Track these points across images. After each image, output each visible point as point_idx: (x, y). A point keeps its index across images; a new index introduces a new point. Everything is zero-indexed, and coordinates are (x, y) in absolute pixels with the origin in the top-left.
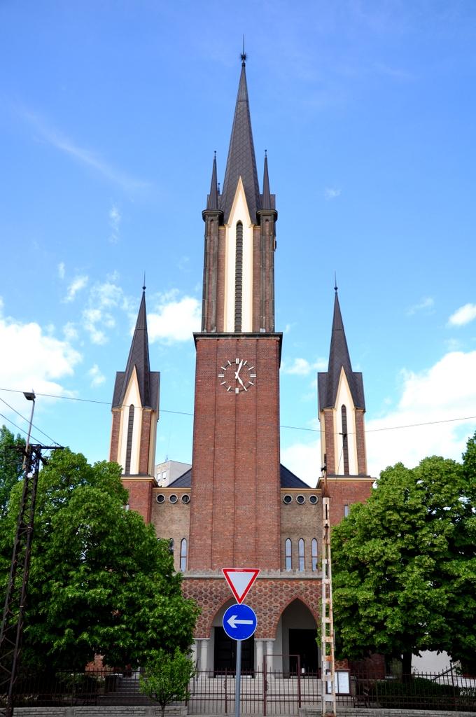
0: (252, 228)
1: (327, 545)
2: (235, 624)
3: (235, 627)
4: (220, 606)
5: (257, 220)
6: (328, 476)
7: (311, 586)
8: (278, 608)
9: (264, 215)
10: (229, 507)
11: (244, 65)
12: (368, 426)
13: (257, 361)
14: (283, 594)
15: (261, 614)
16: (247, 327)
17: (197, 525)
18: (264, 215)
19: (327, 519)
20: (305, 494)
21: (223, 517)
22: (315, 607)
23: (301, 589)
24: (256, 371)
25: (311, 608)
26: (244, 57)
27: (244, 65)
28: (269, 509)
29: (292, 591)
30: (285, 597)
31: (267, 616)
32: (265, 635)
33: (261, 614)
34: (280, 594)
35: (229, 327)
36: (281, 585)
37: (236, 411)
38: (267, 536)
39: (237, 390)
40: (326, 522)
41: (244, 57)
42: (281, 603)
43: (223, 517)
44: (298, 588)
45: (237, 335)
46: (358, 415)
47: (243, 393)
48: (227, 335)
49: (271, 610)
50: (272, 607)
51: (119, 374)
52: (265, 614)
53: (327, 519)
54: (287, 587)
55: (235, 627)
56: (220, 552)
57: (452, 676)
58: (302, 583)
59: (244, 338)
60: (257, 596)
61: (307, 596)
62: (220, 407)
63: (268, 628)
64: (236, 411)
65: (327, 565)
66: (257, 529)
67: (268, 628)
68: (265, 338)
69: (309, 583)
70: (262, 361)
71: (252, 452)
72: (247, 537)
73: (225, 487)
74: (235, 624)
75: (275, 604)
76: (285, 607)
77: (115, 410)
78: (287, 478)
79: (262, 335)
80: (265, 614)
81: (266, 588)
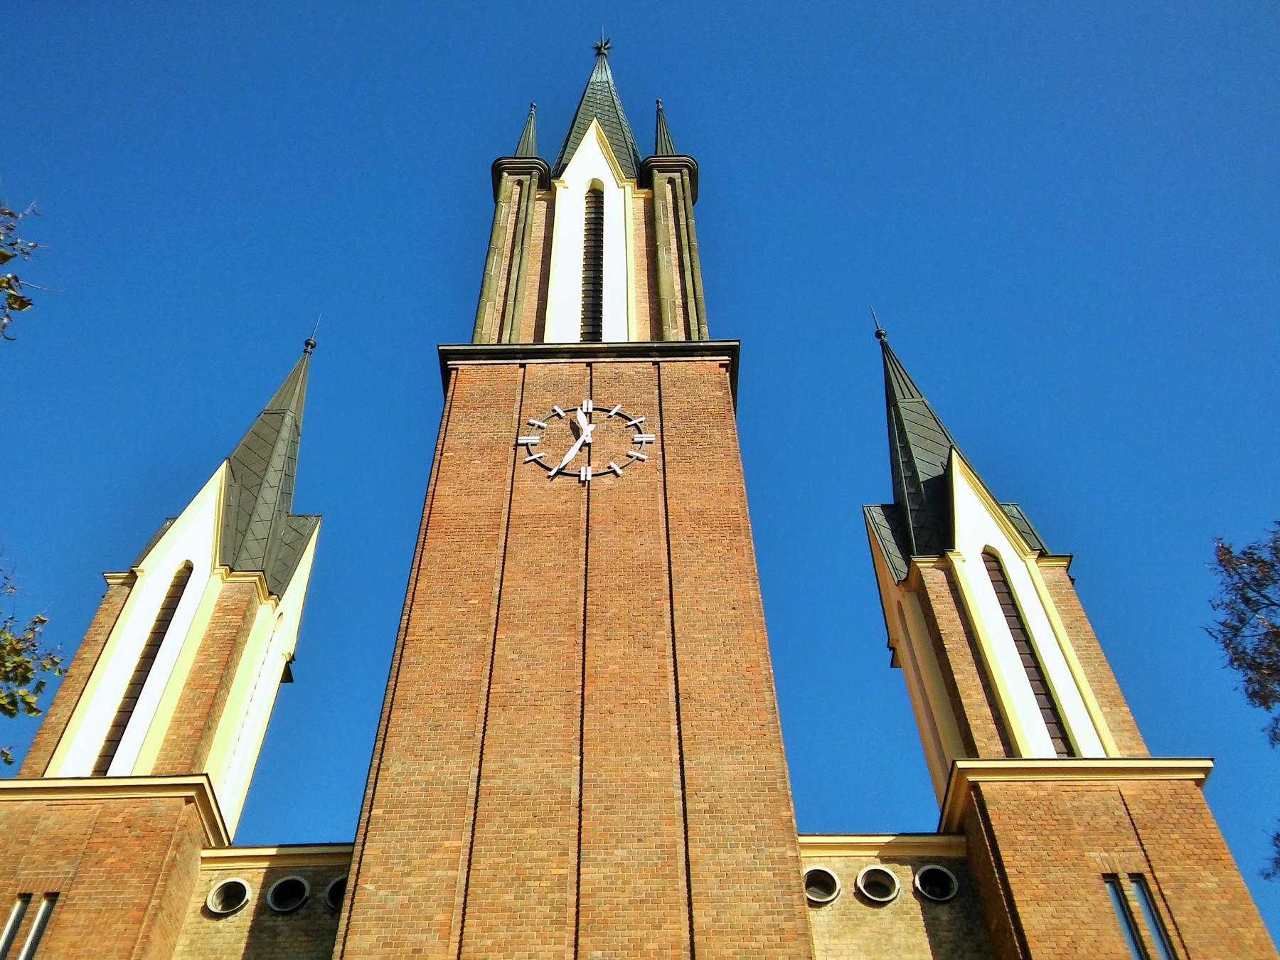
10: (543, 854)
12: (1084, 757)
21: (508, 897)
28: (743, 855)
43: (508, 897)
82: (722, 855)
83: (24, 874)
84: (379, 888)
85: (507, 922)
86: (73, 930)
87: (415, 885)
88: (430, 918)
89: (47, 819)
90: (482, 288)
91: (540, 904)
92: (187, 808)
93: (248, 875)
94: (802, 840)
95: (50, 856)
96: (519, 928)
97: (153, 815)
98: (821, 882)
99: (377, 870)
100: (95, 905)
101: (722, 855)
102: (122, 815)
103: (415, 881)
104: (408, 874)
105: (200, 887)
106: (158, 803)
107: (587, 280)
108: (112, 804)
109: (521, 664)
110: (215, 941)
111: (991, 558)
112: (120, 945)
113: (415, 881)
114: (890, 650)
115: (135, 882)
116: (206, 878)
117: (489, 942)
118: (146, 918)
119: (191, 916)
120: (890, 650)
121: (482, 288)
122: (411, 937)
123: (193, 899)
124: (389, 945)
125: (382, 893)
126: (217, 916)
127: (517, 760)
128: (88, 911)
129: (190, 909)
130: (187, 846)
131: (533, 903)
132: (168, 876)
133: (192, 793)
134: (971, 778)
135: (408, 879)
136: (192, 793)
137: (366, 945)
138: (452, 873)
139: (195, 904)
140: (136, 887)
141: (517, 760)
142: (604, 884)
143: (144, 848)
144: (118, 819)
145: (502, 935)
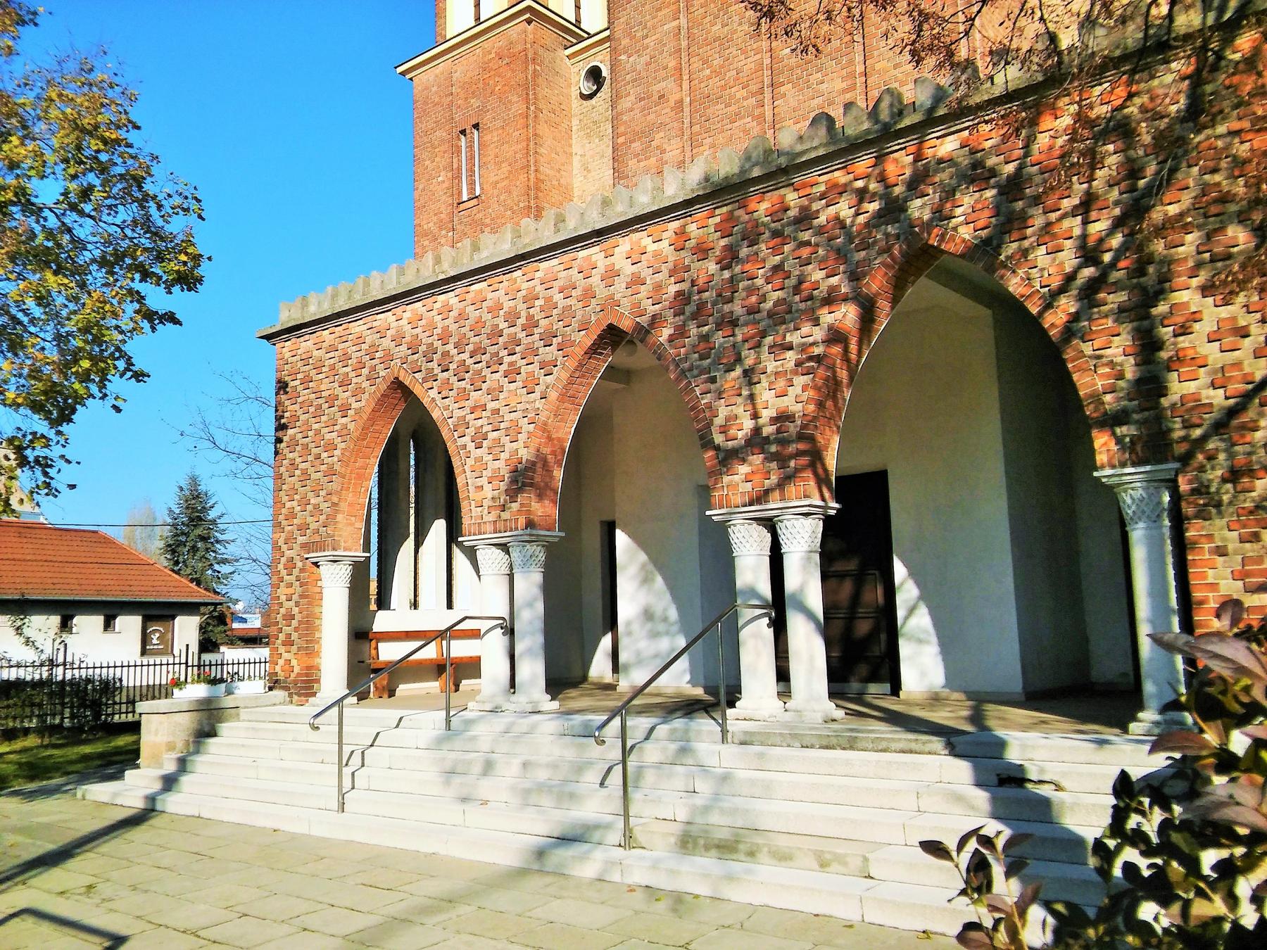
83: (457, 117)
85: (718, 50)
86: (492, 146)
87: (652, 44)
88: (665, 68)
89: (456, 72)
91: (740, 24)
92: (530, 28)
93: (600, 57)
95: (466, 99)
96: (727, 51)
97: (511, 43)
100: (499, 123)
102: (494, 51)
104: (647, 36)
105: (574, 80)
106: (511, 32)
108: (485, 45)
110: (593, 115)
112: (520, 146)
114: (62, 194)
115: (515, 99)
116: (576, 70)
117: (708, 72)
119: (576, 103)
120: (62, 194)
122: (656, 88)
123: (573, 89)
124: (643, 99)
125: (631, 59)
126: (591, 96)
128: (497, 129)
129: (574, 97)
130: (548, 56)
131: (735, 25)
132: (535, 85)
133: (528, 16)
135: (646, 41)
136: (528, 16)
137: (629, 105)
138: (675, 23)
139: (575, 93)
140: (517, 102)
143: (513, 71)
144: (493, 55)
145: (715, 62)
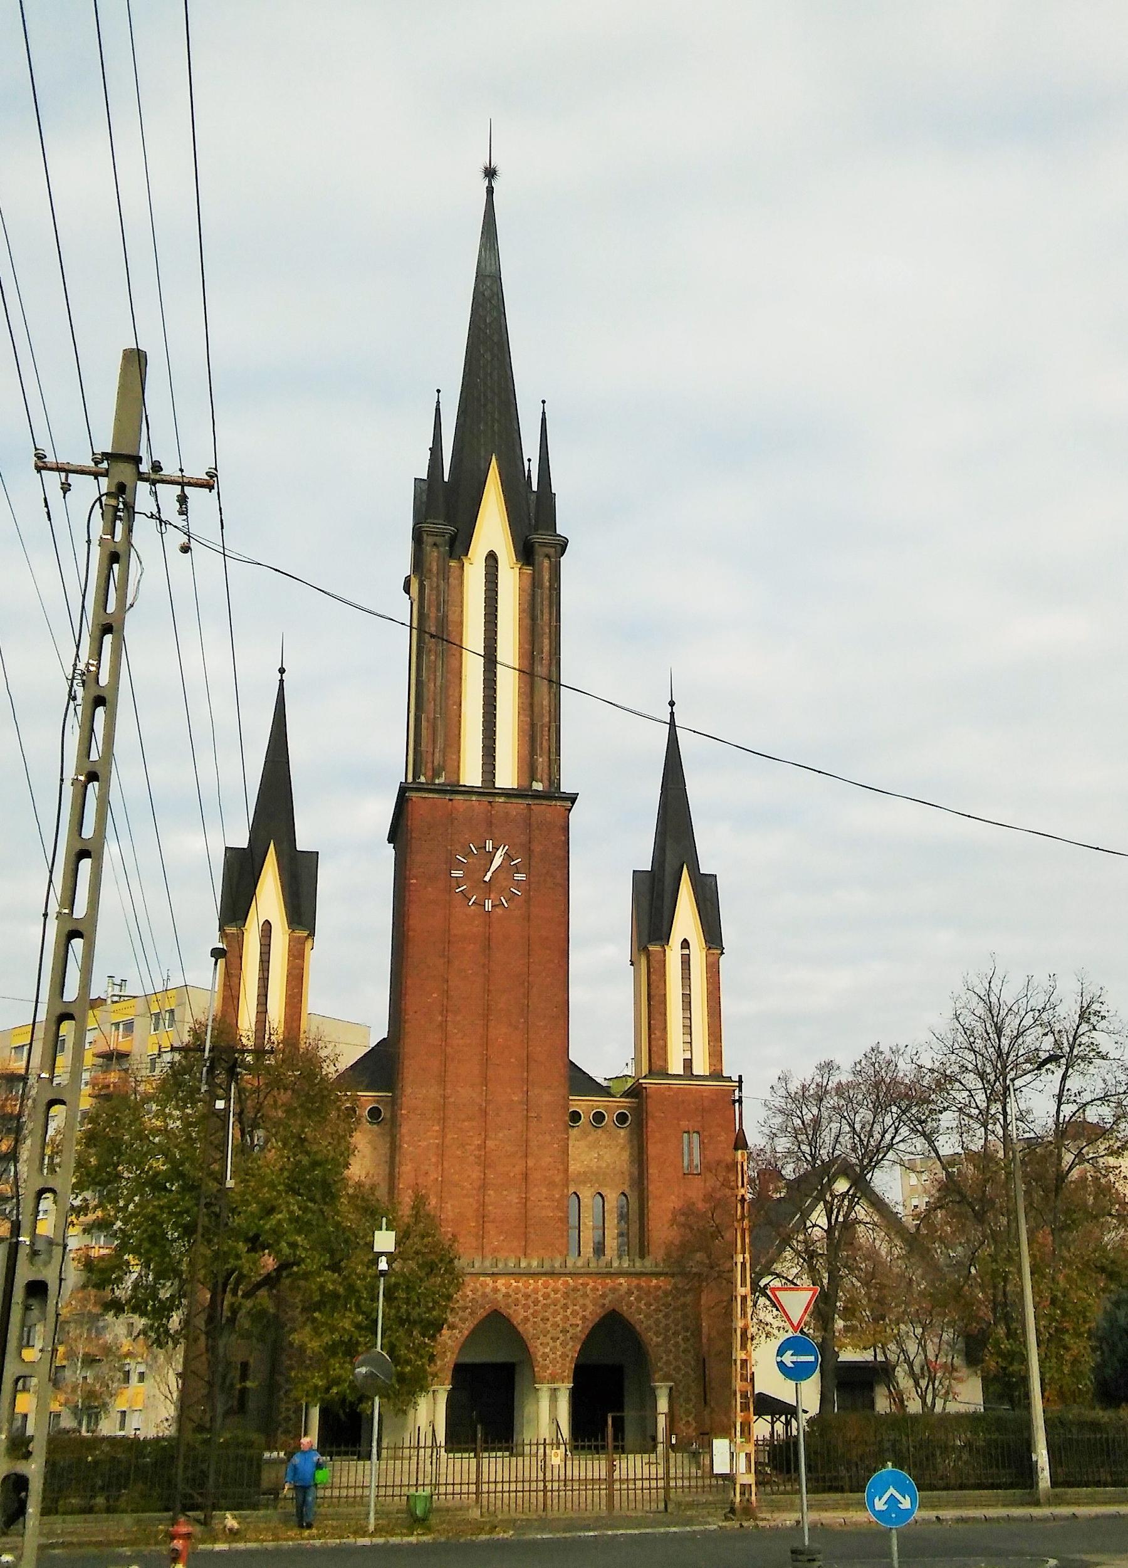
0: (517, 571)
1: (743, 1231)
2: (792, 1362)
3: (792, 1365)
4: (472, 1326)
5: (526, 553)
6: (651, 1073)
7: (639, 1287)
8: (579, 1328)
9: (544, 545)
11: (490, 191)
13: (529, 853)
14: (587, 1302)
15: (548, 1339)
16: (507, 777)
17: (409, 1167)
18: (544, 545)
19: (743, 1186)
20: (607, 1108)
21: (458, 1152)
22: (644, 1326)
23: (621, 1293)
24: (528, 868)
25: (638, 1327)
26: (490, 173)
27: (490, 191)
28: (548, 1138)
29: (603, 1296)
30: (591, 1307)
31: (558, 1342)
32: (553, 1379)
33: (548, 1339)
34: (581, 1301)
35: (471, 775)
36: (585, 1285)
37: (488, 945)
38: (544, 1190)
39: (488, 905)
40: (742, 1191)
41: (490, 173)
42: (584, 1318)
44: (614, 1290)
45: (488, 789)
46: (711, 959)
47: (499, 910)
48: (470, 791)
49: (564, 1331)
50: (567, 1326)
51: (232, 854)
52: (554, 1339)
53: (743, 1186)
54: (594, 1289)
55: (791, 1365)
56: (452, 1220)
57: (628, 1489)
58: (622, 1280)
59: (502, 800)
60: (539, 1308)
61: (630, 1307)
62: (455, 935)
63: (558, 1365)
64: (488, 945)
65: (743, 1264)
66: (526, 1176)
67: (558, 1365)
68: (544, 802)
69: (635, 1282)
70: (537, 848)
71: (516, 1028)
72: (505, 1193)
73: (465, 1094)
74: (792, 1362)
75: (573, 1321)
76: (591, 1326)
77: (231, 930)
78: (581, 1082)
79: (537, 795)
80: (554, 1339)
81: (556, 1291)
82: (540, 1136)
84: (409, 1146)
90: (532, 705)
94: (571, 1098)
98: (575, 1117)
99: (407, 1139)
101: (540, 1136)
103: (424, 1144)
107: (8, 1268)
109: (459, 1035)
111: (492, 558)
113: (424, 1144)
118: (545, 703)
121: (532, 705)
127: (459, 1089)
131: (468, 1154)
134: (644, 1086)
141: (459, 1089)
142: (495, 1148)
